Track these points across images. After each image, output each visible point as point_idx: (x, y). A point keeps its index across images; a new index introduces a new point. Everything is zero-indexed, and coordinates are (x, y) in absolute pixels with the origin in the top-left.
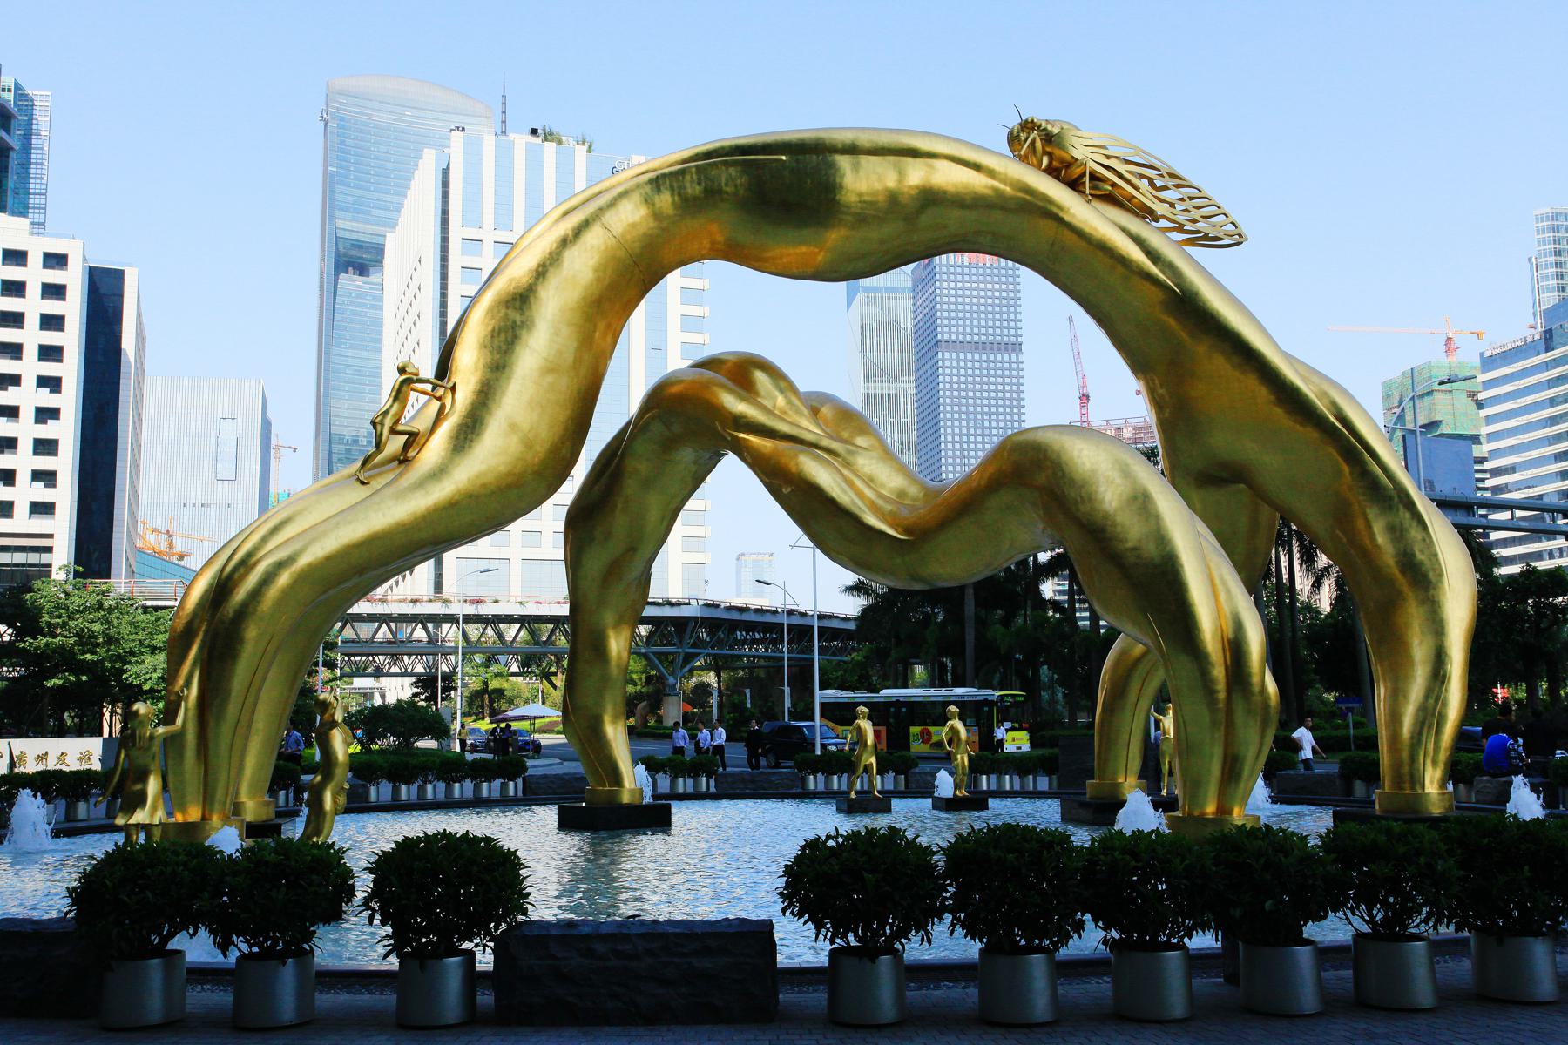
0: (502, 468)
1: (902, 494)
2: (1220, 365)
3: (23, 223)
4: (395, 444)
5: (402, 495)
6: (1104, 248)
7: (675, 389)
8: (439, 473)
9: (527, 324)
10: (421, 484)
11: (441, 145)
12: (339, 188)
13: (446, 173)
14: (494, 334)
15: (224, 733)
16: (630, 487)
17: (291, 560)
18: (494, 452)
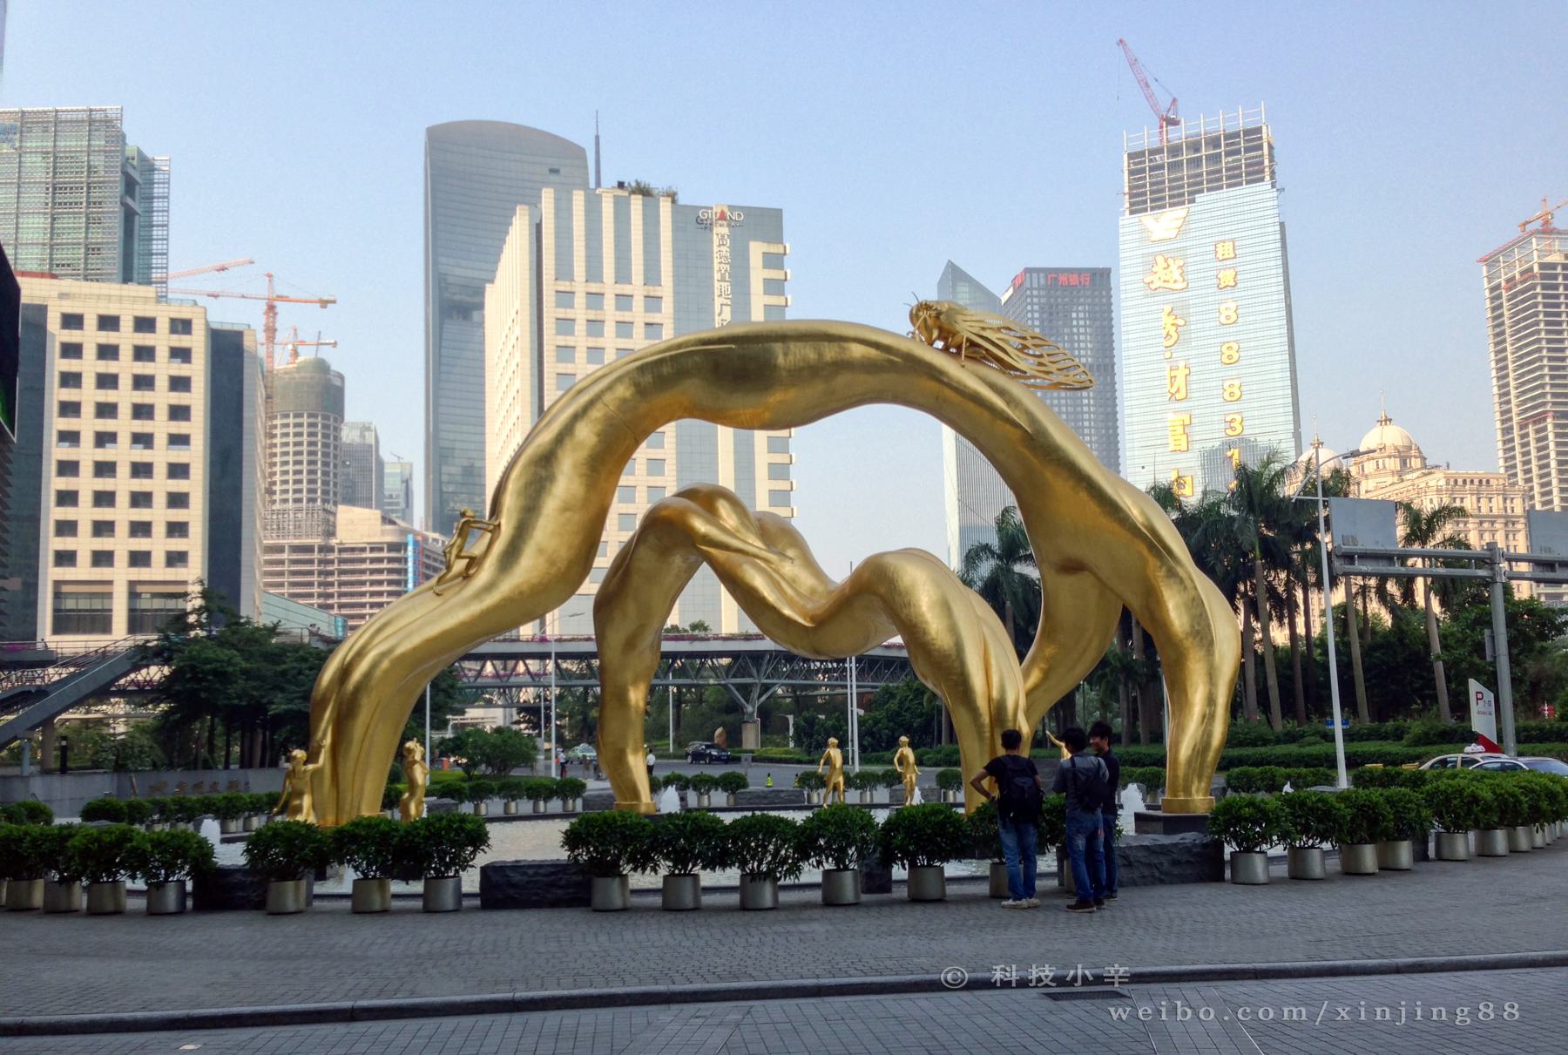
0: (534, 581)
1: (813, 591)
2: (1061, 487)
3: (150, 291)
4: (459, 566)
5: (465, 603)
6: (976, 399)
7: (665, 513)
8: (490, 587)
9: (551, 478)
10: (478, 595)
11: (534, 203)
12: (442, 260)
13: (539, 227)
14: (528, 485)
15: (347, 768)
16: (636, 580)
17: (390, 651)
18: (528, 568)
